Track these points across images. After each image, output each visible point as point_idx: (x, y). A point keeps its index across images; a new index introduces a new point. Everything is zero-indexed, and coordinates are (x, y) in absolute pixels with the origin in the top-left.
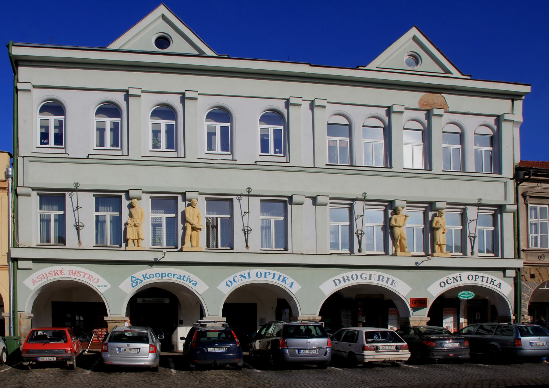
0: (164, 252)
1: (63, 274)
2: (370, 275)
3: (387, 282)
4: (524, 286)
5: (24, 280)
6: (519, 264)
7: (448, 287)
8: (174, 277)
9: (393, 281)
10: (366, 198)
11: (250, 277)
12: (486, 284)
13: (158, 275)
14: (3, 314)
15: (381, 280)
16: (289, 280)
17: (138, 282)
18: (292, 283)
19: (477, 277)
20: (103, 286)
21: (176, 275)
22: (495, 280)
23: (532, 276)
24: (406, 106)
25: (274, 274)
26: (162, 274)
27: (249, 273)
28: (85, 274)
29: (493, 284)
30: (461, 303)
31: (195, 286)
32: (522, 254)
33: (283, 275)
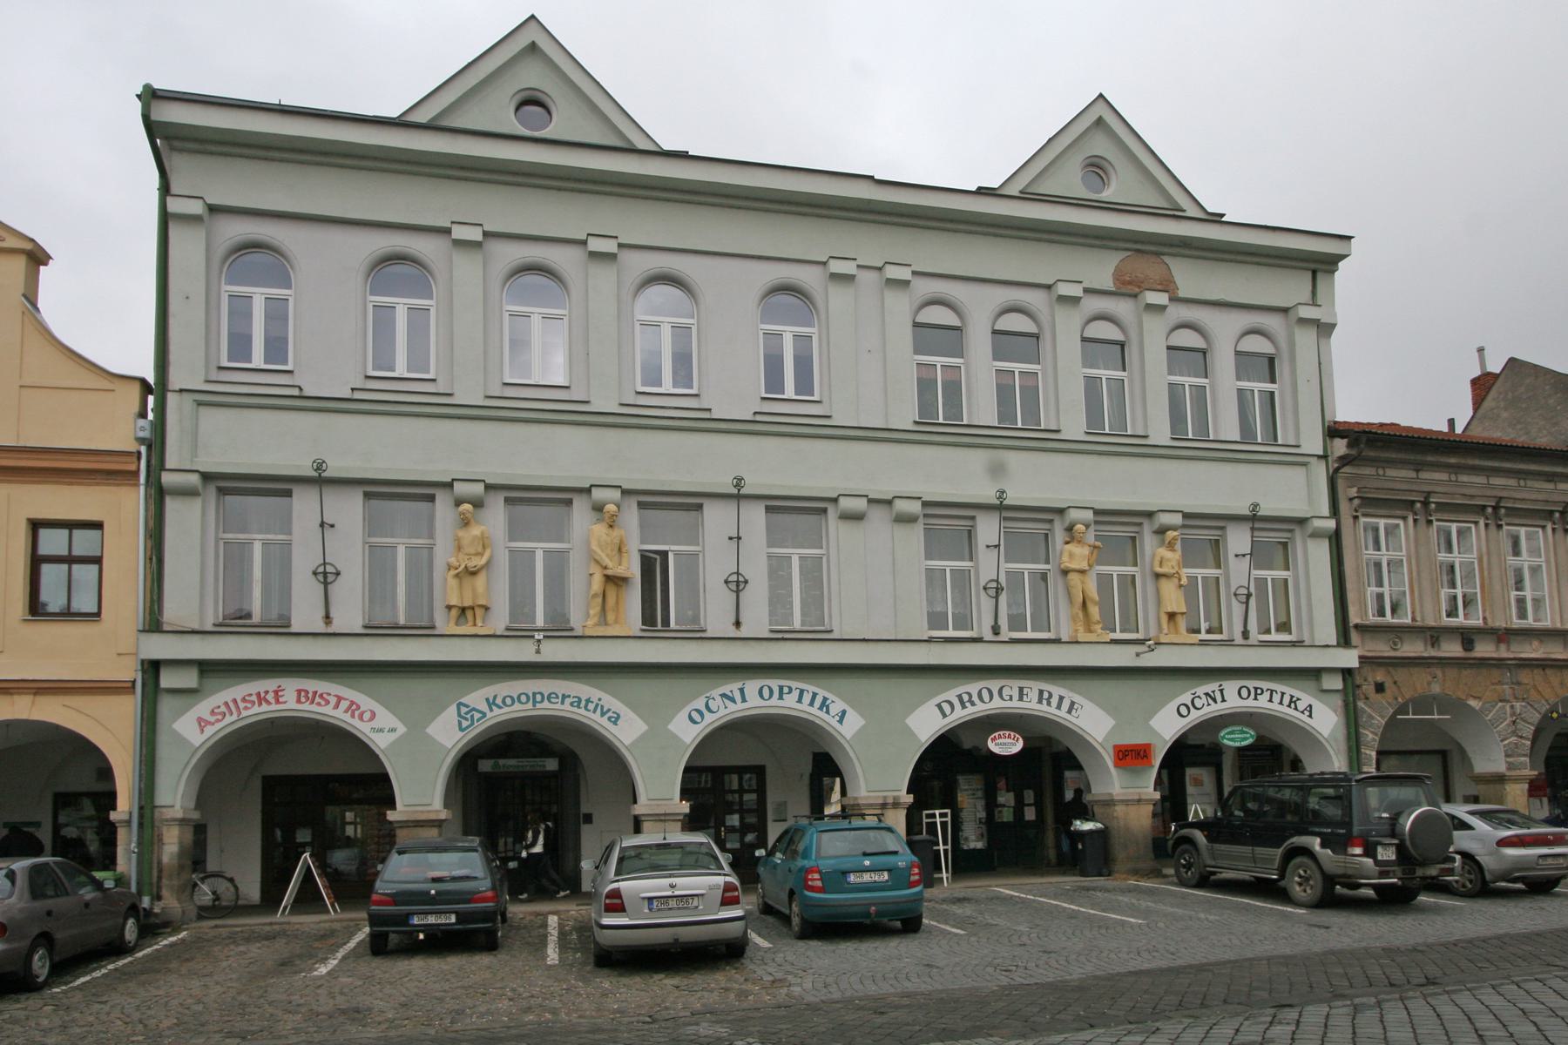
0: (537, 637)
1: (281, 700)
2: (1021, 689)
3: (1059, 707)
4: (1364, 711)
5: (174, 721)
6: (1349, 659)
7: (1195, 716)
8: (563, 703)
9: (1073, 703)
10: (1005, 502)
11: (744, 700)
12: (1280, 708)
13: (523, 698)
14: (113, 816)
15: (1045, 702)
16: (837, 706)
17: (463, 721)
18: (844, 712)
19: (1259, 691)
20: (386, 730)
21: (569, 696)
22: (1298, 699)
23: (1380, 688)
24: (1087, 284)
25: (802, 691)
26: (534, 694)
27: (742, 690)
28: (340, 699)
29: (1296, 709)
30: (1224, 756)
31: (615, 723)
32: (1355, 637)
33: (822, 693)
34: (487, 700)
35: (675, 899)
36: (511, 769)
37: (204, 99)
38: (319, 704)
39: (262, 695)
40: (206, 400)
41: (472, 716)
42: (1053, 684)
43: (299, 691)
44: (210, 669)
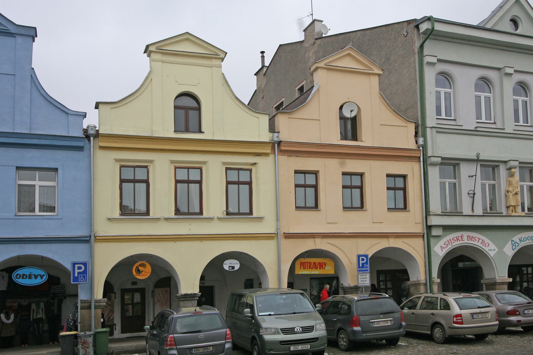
13: (529, 238)
17: (513, 247)
20: (492, 250)
34: (519, 239)
35: (202, 348)
36: (469, 266)
37: (439, 20)
38: (473, 241)
39: (458, 238)
40: (440, 130)
41: (516, 245)
42: (477, 233)
43: (468, 236)
44: (447, 228)
